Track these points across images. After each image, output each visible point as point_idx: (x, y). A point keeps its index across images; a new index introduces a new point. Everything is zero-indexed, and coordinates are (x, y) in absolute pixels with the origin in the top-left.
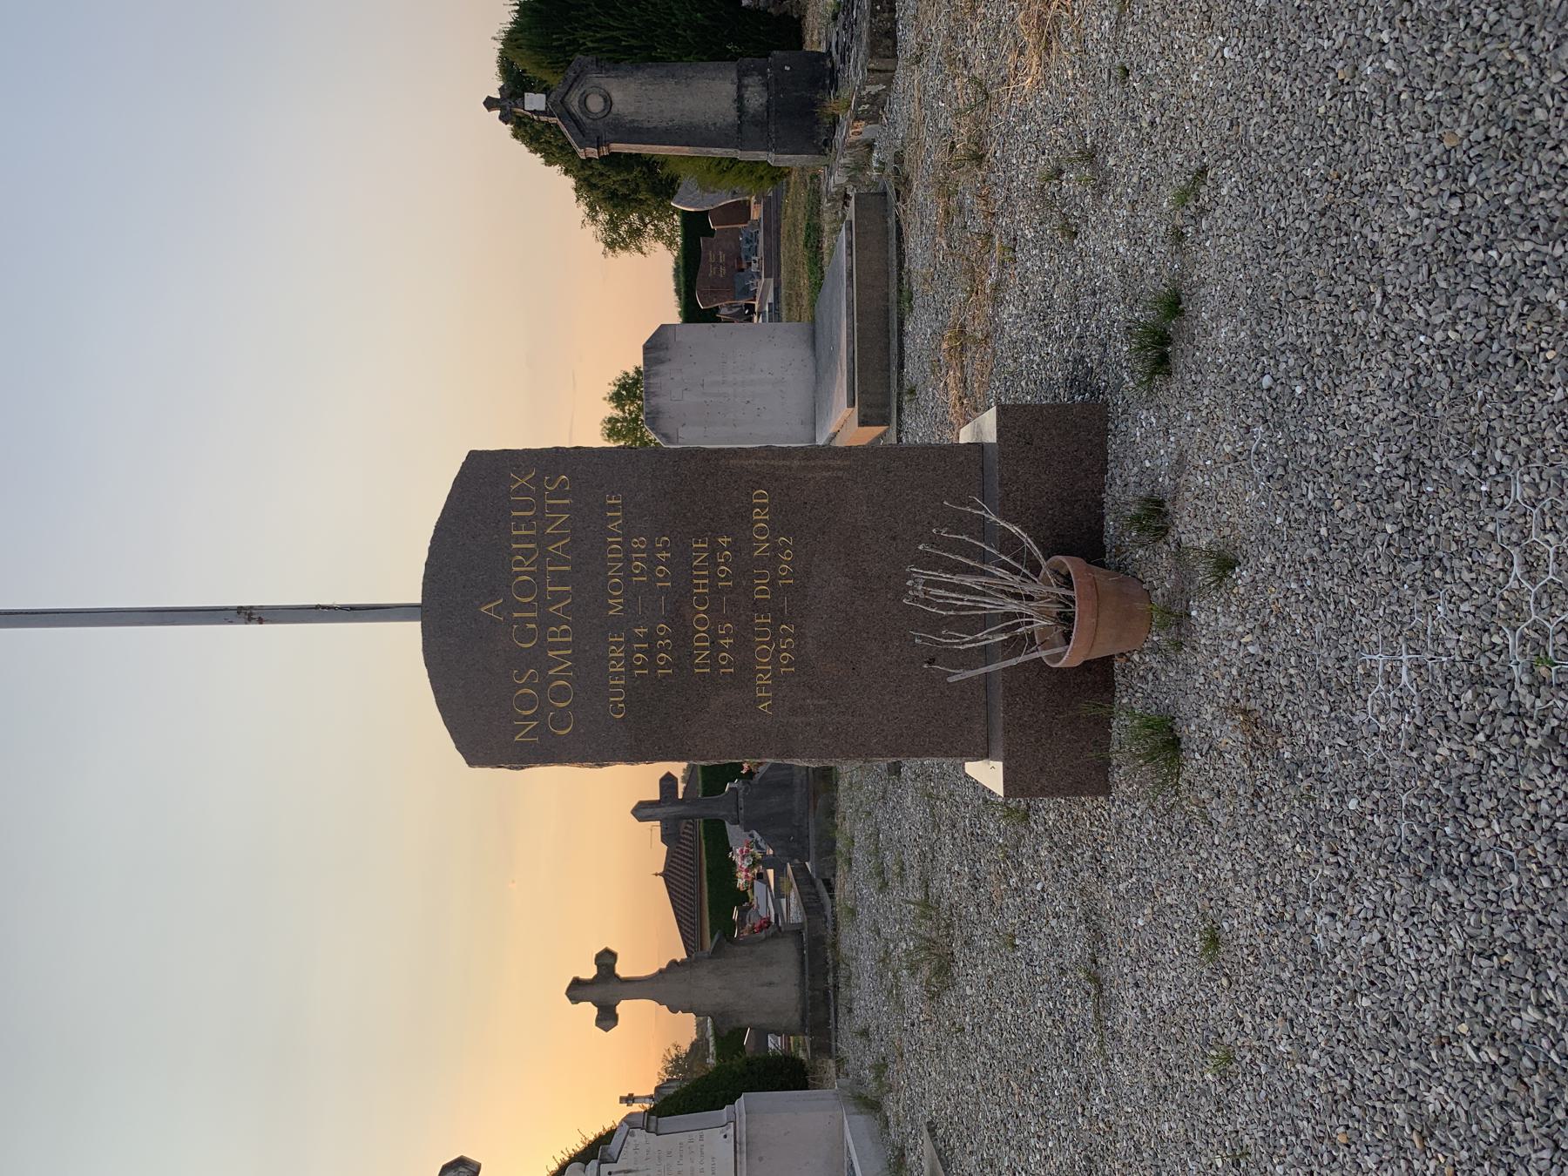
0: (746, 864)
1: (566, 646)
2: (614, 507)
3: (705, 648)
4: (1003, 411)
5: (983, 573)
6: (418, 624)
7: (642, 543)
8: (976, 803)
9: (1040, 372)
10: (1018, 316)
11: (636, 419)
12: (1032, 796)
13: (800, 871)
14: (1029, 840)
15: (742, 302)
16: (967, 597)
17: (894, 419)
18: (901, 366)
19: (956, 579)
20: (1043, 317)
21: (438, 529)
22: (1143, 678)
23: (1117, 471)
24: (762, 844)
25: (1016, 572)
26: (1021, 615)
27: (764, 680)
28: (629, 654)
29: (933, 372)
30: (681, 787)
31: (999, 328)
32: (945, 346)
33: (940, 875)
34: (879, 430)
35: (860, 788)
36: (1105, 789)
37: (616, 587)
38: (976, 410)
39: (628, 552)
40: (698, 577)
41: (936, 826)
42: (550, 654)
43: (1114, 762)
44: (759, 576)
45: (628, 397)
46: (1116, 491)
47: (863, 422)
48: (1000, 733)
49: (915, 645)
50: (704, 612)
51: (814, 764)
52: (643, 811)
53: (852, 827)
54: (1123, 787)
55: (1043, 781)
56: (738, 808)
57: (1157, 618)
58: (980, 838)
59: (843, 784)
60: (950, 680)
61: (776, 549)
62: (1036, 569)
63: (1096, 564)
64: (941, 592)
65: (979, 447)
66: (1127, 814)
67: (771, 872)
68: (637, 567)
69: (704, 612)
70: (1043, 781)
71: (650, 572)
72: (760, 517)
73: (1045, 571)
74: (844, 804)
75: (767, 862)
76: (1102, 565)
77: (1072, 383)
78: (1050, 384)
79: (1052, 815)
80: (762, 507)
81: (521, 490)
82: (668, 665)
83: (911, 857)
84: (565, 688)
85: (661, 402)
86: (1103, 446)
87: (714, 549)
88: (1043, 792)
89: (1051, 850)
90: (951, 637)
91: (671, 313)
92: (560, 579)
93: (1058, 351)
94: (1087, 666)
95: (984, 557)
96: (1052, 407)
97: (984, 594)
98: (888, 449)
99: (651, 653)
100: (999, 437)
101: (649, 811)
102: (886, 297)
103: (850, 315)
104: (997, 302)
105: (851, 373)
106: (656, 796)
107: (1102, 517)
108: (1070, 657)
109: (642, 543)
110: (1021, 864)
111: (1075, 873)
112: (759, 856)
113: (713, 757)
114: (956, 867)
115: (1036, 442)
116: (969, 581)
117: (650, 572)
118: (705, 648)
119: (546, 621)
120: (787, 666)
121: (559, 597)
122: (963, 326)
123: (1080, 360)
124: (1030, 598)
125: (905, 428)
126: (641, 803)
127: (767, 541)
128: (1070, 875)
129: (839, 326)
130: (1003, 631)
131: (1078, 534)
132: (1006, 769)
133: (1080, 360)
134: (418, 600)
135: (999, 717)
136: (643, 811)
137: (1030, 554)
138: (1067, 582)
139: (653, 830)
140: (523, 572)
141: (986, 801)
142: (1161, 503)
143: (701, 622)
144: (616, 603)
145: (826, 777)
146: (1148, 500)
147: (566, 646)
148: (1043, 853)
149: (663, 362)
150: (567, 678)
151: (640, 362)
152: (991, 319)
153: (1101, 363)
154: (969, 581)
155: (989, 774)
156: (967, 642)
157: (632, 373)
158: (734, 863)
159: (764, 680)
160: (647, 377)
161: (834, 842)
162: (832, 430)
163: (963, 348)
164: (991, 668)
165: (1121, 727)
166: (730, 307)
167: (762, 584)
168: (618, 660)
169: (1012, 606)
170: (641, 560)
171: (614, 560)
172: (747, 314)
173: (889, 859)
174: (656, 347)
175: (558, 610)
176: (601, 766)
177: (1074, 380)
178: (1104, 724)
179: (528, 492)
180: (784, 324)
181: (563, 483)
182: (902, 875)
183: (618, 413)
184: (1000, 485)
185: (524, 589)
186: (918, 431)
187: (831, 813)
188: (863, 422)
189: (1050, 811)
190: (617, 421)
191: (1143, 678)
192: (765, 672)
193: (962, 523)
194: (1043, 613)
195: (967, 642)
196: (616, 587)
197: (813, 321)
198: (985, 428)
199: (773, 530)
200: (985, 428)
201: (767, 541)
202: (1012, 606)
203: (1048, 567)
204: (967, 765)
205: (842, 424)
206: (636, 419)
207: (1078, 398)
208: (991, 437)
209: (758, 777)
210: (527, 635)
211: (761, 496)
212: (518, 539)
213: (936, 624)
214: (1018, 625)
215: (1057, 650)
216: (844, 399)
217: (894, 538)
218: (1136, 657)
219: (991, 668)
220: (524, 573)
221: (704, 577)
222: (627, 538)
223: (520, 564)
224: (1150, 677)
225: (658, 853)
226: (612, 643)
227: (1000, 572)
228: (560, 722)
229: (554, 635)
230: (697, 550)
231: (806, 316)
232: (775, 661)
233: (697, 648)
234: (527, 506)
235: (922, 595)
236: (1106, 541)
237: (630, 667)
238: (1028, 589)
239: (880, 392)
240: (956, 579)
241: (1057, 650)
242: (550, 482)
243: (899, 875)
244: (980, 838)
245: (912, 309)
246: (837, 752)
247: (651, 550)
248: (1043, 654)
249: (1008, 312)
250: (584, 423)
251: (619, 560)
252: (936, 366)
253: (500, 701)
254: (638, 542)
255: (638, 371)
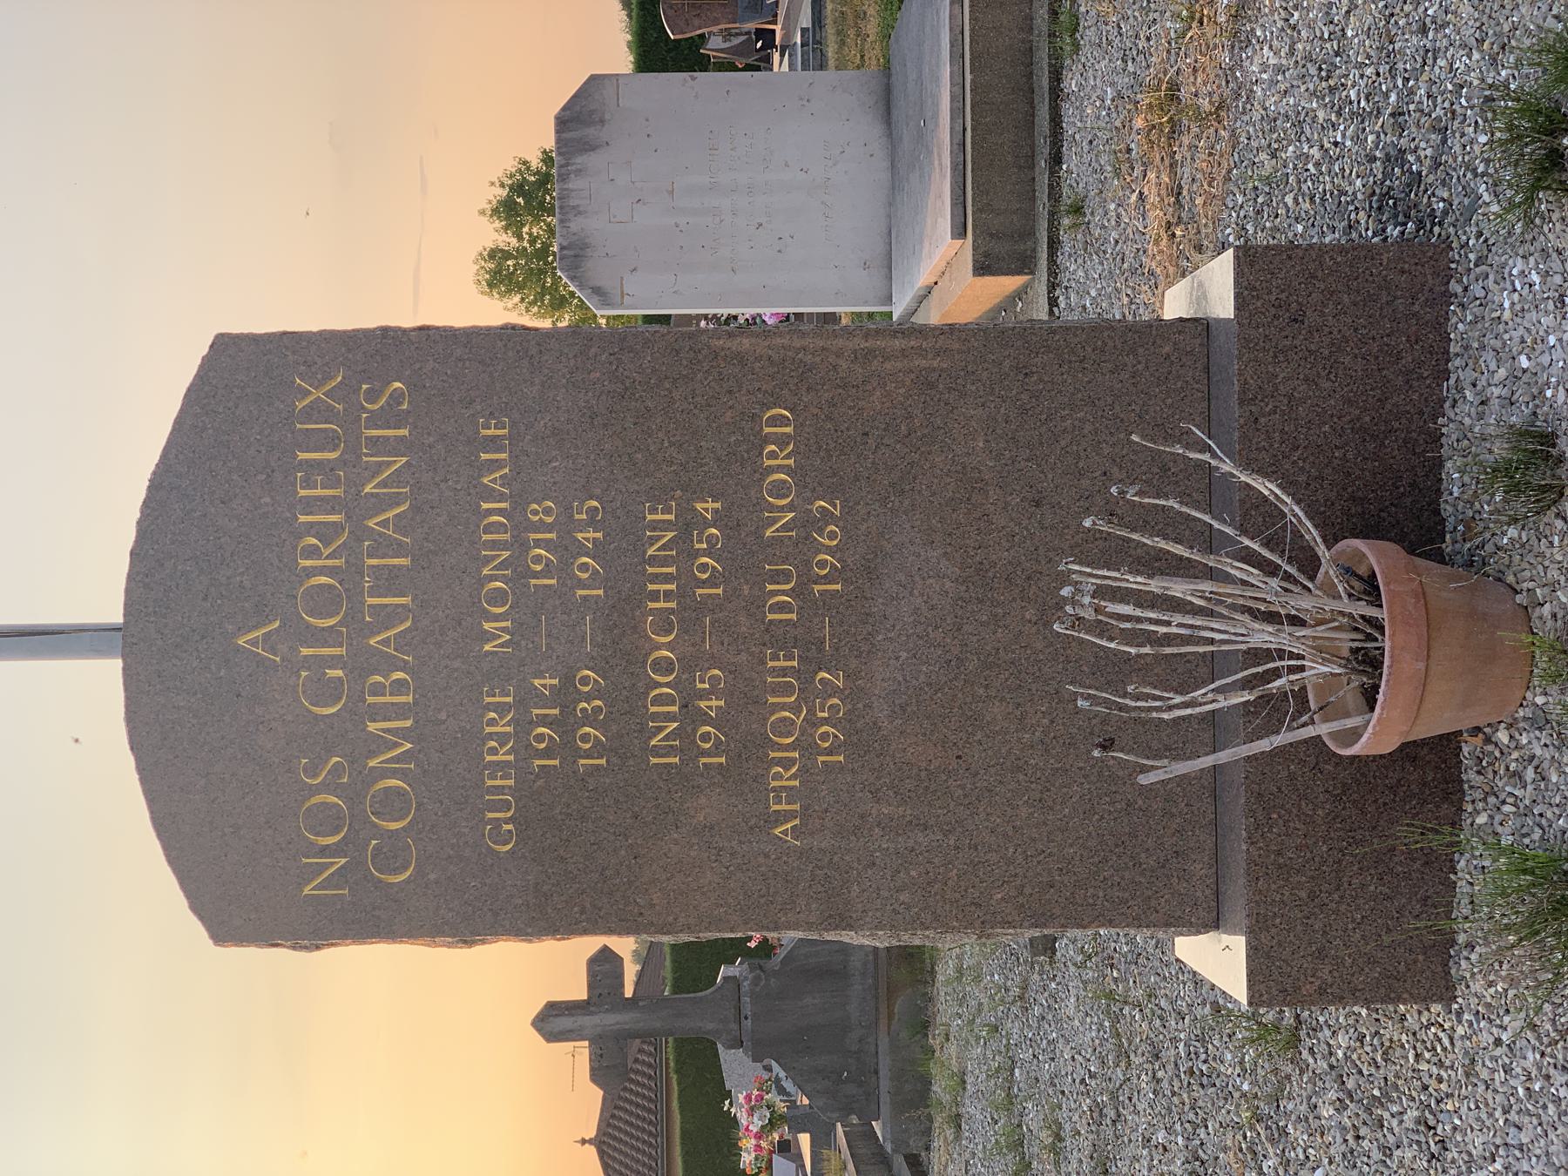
0: (756, 1125)
1: (400, 711)
2: (493, 443)
3: (669, 717)
4: (1247, 259)
5: (1211, 574)
6: (116, 665)
7: (547, 511)
8: (1199, 1012)
9: (1318, 182)
10: (1280, 70)
11: (544, 252)
12: (1307, 1002)
13: (862, 1139)
14: (1299, 1086)
15: (751, 26)
16: (1178, 618)
17: (1043, 263)
18: (1056, 159)
19: (1155, 585)
20: (1327, 72)
21: (155, 485)
22: (1517, 776)
23: (1467, 376)
24: (788, 1085)
25: (1270, 570)
26: (1281, 654)
27: (785, 778)
28: (524, 725)
29: (1117, 173)
30: (631, 971)
31: (1242, 92)
32: (1139, 123)
33: (1129, 1151)
34: (1011, 283)
35: (977, 979)
36: (1444, 990)
37: (498, 597)
38: (1199, 248)
39: (520, 527)
40: (656, 578)
41: (1123, 1055)
42: (372, 763)
43: (1461, 938)
44: (776, 577)
45: (529, 207)
46: (1465, 412)
47: (983, 268)
48: (1242, 881)
49: (1078, 711)
50: (658, 647)
51: (882, 940)
52: (554, 1021)
53: (961, 1054)
54: (1477, 986)
55: (1325, 974)
56: (739, 1017)
57: (1542, 661)
58: (1206, 1080)
59: (945, 971)
60: (1144, 780)
61: (808, 524)
62: (1310, 565)
63: (1426, 556)
64: (1126, 609)
65: (1200, 328)
66: (1486, 1039)
67: (805, 1140)
68: (538, 559)
69: (670, 646)
70: (1325, 974)
71: (563, 569)
72: (778, 462)
73: (1327, 570)
74: (946, 1010)
75: (799, 1121)
76: (1440, 558)
77: (1381, 201)
78: (1340, 201)
79: (1342, 1039)
80: (782, 441)
81: (315, 411)
82: (598, 750)
83: (1075, 1115)
84: (398, 792)
85: (591, 225)
86: (1440, 328)
87: (688, 525)
88: (1325, 996)
89: (1340, 1105)
90: (1147, 697)
91: (613, 50)
92: (389, 581)
93: (1356, 139)
94: (1409, 752)
95: (1210, 541)
96: (1342, 250)
97: (1211, 614)
98: (1029, 329)
99: (565, 724)
100: (1237, 308)
101: (566, 1022)
102: (1028, 25)
103: (957, 56)
104: (1241, 41)
105: (959, 170)
106: (580, 993)
107: (1439, 463)
108: (1376, 736)
109: (547, 511)
110: (1283, 1132)
111: (1387, 1151)
112: (782, 1107)
113: (688, 928)
114: (1161, 1137)
115: (1312, 317)
116: (1179, 589)
117: (563, 569)
118: (669, 717)
119: (363, 664)
120: (829, 752)
121: (388, 617)
122: (1174, 87)
123: (1397, 157)
124: (1296, 621)
125: (1064, 278)
126: (551, 1006)
127: (791, 507)
128: (1376, 1155)
129: (936, 80)
130: (1247, 684)
131: (1392, 498)
132: (1253, 952)
133: (1397, 157)
134: (118, 618)
135: (1239, 850)
136: (554, 1021)
137: (1297, 535)
138: (1370, 589)
139: (573, 1059)
140: (318, 569)
141: (1217, 1008)
142: (1549, 439)
143: (664, 667)
144: (497, 630)
145: (913, 965)
146: (1523, 434)
147: (400, 711)
148: (1326, 1111)
149: (593, 149)
150: (403, 775)
151: (550, 142)
152: (1228, 74)
153: (1437, 164)
154: (1179, 589)
155: (1219, 959)
156: (1175, 707)
157: (535, 163)
158: (735, 1121)
159: (785, 778)
160: (563, 178)
161: (927, 1082)
162: (923, 278)
163: (1175, 129)
164: (1223, 757)
165: (1473, 874)
166: (728, 34)
167: (780, 593)
168: (502, 739)
169: (1264, 636)
170: (546, 544)
171: (494, 545)
172: (756, 54)
173: (1033, 1118)
174: (581, 119)
175: (386, 642)
176: (468, 943)
177: (1387, 194)
178: (1442, 865)
179: (328, 415)
180: (829, 75)
181: (397, 398)
182: (1056, 1148)
183: (508, 241)
184: (1241, 402)
185: (323, 601)
186: (1091, 290)
187: (923, 1026)
188: (983, 268)
189: (1339, 1030)
190: (507, 255)
191: (1517, 776)
192: (787, 764)
193: (1165, 476)
194: (1324, 651)
195: (1175, 707)
196: (498, 597)
197: (887, 70)
198: (1210, 291)
199: (802, 485)
200: (1210, 291)
201: (791, 507)
202: (1264, 636)
203: (1334, 561)
204: (1180, 942)
205: (942, 277)
206: (544, 252)
207: (1393, 232)
208: (1223, 306)
209: (781, 954)
210: (330, 692)
211: (779, 422)
212: (310, 505)
213: (1115, 672)
214: (1276, 674)
215: (1350, 723)
216: (945, 223)
217: (1038, 504)
218: (1503, 736)
219: (1223, 757)
220: (322, 571)
221: (667, 578)
222: (519, 502)
223: (313, 552)
224: (1530, 774)
225: (586, 1104)
226: (488, 708)
227: (1238, 569)
228: (390, 857)
229: (378, 690)
230: (654, 526)
231: (874, 54)
232: (807, 747)
233: (655, 717)
234: (331, 442)
235: (1088, 614)
236: (1447, 510)
237: (525, 751)
238: (1303, 603)
239: (1016, 203)
240: (1155, 585)
241: (1350, 723)
242: (372, 396)
243: (1053, 1149)
244: (1206, 1080)
245: (1077, 47)
246: (927, 917)
247: (566, 525)
248: (1322, 729)
249: (1262, 60)
250: (442, 279)
251: (504, 546)
252: (1123, 161)
253: (275, 837)
254: (538, 511)
255: (547, 159)
